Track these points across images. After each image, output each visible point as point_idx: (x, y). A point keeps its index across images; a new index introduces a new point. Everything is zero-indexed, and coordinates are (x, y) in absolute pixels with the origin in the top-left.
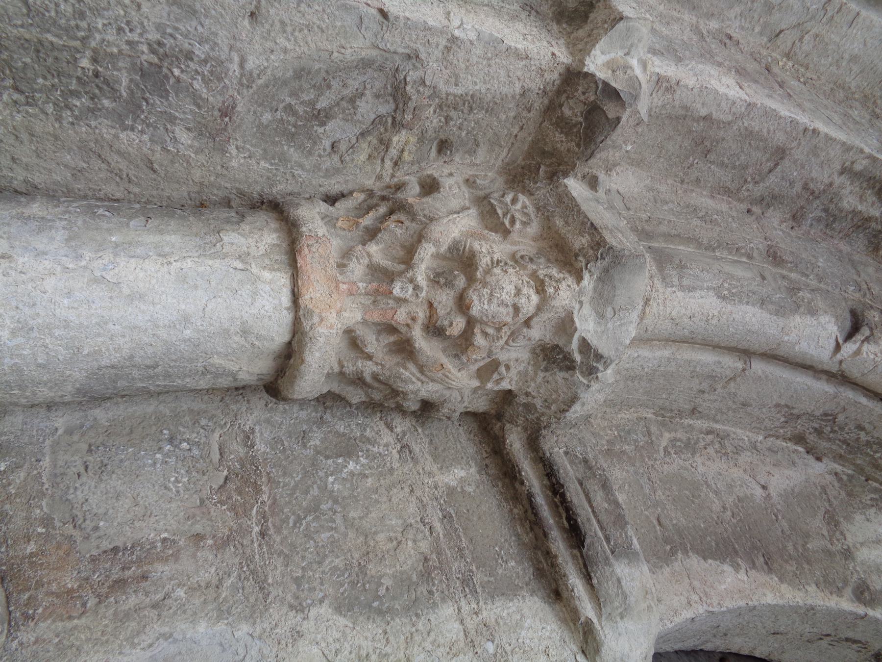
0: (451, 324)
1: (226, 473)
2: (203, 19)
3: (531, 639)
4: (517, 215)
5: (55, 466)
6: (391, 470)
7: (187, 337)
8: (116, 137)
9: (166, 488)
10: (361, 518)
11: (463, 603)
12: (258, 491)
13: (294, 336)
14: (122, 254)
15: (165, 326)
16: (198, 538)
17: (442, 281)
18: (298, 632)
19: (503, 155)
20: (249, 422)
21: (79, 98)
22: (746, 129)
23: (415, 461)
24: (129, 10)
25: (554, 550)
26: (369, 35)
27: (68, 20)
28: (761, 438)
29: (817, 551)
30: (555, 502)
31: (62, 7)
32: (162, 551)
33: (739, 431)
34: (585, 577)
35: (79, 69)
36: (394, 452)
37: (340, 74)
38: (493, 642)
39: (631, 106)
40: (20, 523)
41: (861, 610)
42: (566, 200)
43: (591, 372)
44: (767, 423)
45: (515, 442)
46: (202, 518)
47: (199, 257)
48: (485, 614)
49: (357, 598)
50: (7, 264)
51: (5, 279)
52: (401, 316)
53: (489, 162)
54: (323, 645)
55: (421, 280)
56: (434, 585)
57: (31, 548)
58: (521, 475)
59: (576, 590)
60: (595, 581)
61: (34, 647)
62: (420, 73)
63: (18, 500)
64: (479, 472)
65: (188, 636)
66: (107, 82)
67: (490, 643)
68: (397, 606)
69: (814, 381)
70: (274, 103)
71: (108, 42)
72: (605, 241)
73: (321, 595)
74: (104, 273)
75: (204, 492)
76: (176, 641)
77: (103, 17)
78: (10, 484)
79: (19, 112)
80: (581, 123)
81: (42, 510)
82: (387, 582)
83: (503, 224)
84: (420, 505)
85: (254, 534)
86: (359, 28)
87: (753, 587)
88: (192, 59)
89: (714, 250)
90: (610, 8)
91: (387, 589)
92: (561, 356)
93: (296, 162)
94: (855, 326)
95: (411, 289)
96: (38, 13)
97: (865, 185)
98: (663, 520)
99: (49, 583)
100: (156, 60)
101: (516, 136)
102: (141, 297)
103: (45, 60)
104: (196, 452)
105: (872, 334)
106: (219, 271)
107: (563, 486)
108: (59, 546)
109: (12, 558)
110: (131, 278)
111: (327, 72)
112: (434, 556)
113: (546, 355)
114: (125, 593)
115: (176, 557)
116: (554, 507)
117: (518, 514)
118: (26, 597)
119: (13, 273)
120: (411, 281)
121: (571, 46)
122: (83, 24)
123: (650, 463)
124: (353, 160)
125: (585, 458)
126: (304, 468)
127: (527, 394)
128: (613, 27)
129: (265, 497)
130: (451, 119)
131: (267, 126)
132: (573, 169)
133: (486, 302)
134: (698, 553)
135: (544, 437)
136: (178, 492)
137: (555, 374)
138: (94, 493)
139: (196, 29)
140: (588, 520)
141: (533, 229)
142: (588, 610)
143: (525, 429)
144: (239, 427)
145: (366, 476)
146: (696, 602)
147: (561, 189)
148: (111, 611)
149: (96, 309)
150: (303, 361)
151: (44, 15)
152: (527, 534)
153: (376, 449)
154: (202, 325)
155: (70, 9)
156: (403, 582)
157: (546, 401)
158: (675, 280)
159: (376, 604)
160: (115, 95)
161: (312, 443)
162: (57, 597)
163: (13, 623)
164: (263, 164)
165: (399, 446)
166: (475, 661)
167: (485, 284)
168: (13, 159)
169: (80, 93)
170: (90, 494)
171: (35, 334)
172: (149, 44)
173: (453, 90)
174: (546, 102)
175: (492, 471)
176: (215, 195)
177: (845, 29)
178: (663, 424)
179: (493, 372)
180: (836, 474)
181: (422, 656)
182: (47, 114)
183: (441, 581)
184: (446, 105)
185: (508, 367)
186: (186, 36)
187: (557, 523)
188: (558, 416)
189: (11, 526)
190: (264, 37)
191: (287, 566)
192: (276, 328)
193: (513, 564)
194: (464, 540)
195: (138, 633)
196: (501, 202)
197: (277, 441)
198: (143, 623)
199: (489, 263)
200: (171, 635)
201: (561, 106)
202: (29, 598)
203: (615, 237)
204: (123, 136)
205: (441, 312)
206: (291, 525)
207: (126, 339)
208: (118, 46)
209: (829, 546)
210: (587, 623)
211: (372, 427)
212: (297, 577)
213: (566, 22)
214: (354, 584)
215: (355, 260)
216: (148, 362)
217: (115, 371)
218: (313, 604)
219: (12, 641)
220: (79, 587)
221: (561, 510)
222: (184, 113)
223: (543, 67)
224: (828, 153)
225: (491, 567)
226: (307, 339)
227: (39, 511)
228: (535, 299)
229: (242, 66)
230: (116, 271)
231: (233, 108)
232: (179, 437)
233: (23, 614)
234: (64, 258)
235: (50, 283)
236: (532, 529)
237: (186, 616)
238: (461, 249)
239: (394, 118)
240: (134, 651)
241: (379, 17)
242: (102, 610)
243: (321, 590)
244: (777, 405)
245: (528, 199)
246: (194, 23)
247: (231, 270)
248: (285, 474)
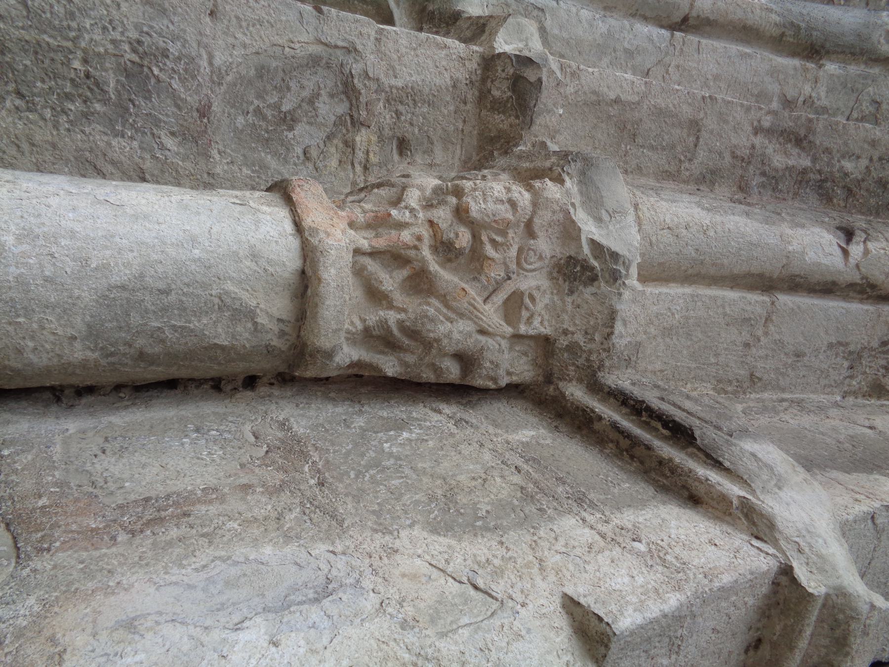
0: (457, 235)
2: (172, 17)
7: (197, 257)
8: (109, 144)
13: (305, 261)
24: (111, 9)
26: (310, 29)
27: (61, 21)
30: (645, 422)
34: (714, 466)
35: (72, 71)
37: (295, 73)
39: (545, 66)
43: (615, 277)
57: (43, 501)
59: (711, 478)
60: (727, 464)
66: (97, 84)
71: (96, 41)
77: (90, 17)
79: (20, 118)
80: (511, 97)
86: (301, 23)
88: (167, 57)
92: (578, 268)
93: (275, 169)
96: (36, 14)
97: (781, 139)
101: (463, 131)
102: (146, 217)
103: (43, 62)
111: (284, 71)
113: (565, 274)
116: (646, 426)
122: (74, 24)
124: (326, 166)
127: (565, 332)
130: (401, 114)
132: (521, 139)
139: (168, 27)
142: (735, 490)
143: (580, 380)
151: (41, 16)
152: (630, 464)
155: (62, 10)
157: (586, 333)
160: (105, 102)
169: (73, 96)
172: (130, 43)
173: (393, 82)
174: (477, 93)
177: (696, 56)
179: (520, 308)
182: (45, 120)
185: (532, 298)
186: (160, 35)
188: (606, 346)
201: (489, 91)
205: (443, 225)
207: (135, 254)
208: (104, 46)
210: (742, 503)
216: (161, 285)
217: (125, 295)
219: (22, 569)
221: (654, 423)
222: (167, 115)
223: (462, 55)
224: (734, 118)
226: (318, 254)
229: (211, 64)
231: (210, 107)
239: (351, 116)
244: (831, 346)
245: (475, 44)
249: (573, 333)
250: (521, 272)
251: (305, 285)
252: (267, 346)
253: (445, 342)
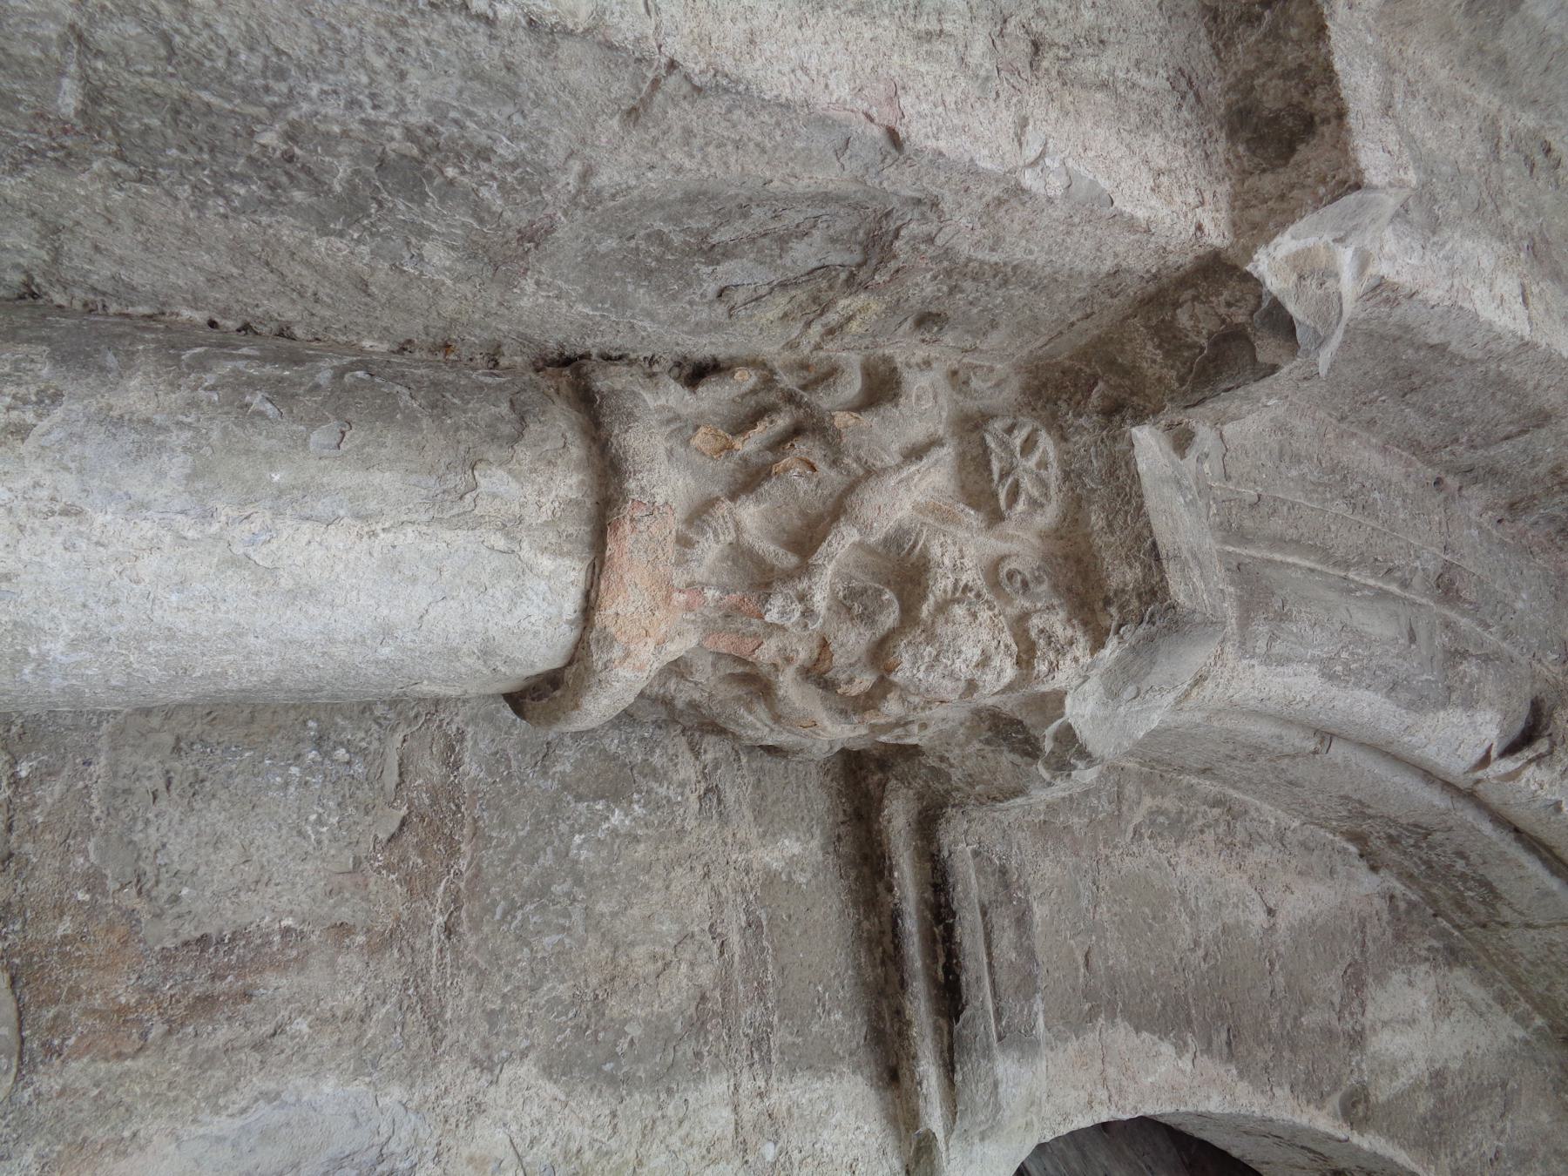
0: (850, 681)
1: (404, 811)
2: (528, 106)
3: (835, 1145)
4: (1027, 483)
5: (115, 774)
6: (681, 832)
8: (307, 242)
9: (300, 833)
10: (614, 915)
11: (745, 1077)
12: (453, 851)
13: (570, 663)
14: (289, 511)
15: (346, 641)
16: (343, 930)
17: (857, 608)
18: (479, 1105)
19: (1036, 344)
20: (457, 719)
21: (245, 183)
22: (1500, 374)
23: (724, 819)
25: (909, 1012)
28: (1296, 824)
29: (1313, 1030)
31: (243, 57)
32: (281, 952)
33: (1266, 807)
34: (945, 1065)
36: (693, 798)
38: (776, 1143)
39: (1308, 353)
40: (48, 880)
41: (1342, 1132)
42: (1122, 473)
44: (1317, 811)
45: (898, 815)
46: (353, 894)
47: (428, 524)
48: (775, 1096)
49: (581, 1054)
50: (73, 527)
51: (67, 555)
52: (767, 652)
54: (514, 1128)
55: (820, 601)
56: (706, 1043)
57: (65, 927)
58: (891, 874)
59: (925, 1085)
60: (958, 1077)
61: (59, 1102)
62: (931, 228)
63: (48, 837)
64: (824, 848)
65: (305, 1098)
67: (770, 1146)
68: (641, 1074)
69: (1422, 785)
72: (1165, 589)
73: (525, 1043)
74: (250, 550)
75: (363, 846)
76: (284, 1105)
78: (34, 806)
80: (1202, 349)
81: (87, 858)
82: (634, 1030)
83: (995, 495)
84: (714, 900)
85: (434, 931)
87: (1195, 1083)
89: (1348, 568)
90: (1345, 152)
91: (632, 1042)
94: (1526, 736)
95: (797, 614)
98: (1094, 959)
99: (90, 993)
100: (415, 152)
104: (359, 768)
105: (1551, 752)
106: (461, 552)
107: (954, 915)
108: (110, 929)
109: (32, 944)
110: (300, 559)
112: (717, 994)
114: (212, 1019)
115: (302, 963)
116: (929, 941)
117: (869, 931)
118: (51, 1015)
119: (82, 544)
120: (802, 598)
121: (1241, 202)
123: (1104, 851)
125: (1003, 866)
126: (536, 815)
128: (1335, 199)
129: (463, 864)
131: (604, 256)
133: (923, 668)
134: (1130, 1020)
135: (948, 822)
136: (319, 842)
137: (1001, 752)
138: (177, 834)
140: (978, 979)
141: (1048, 517)
142: (934, 1118)
143: (920, 797)
144: (440, 727)
145: (637, 839)
146: (1101, 1103)
147: (1122, 446)
148: (186, 1050)
149: (227, 612)
150: (577, 706)
151: (200, 64)
152: (874, 967)
153: (662, 791)
156: (661, 1033)
158: (1261, 645)
159: (608, 1067)
161: (559, 768)
162: (102, 1019)
163: (27, 1059)
164: (580, 307)
165: (703, 786)
166: (741, 1175)
167: (931, 638)
168: (96, 248)
169: (250, 177)
170: (172, 834)
171: (111, 646)
175: (844, 849)
178: (1147, 781)
180: (1392, 897)
181: (663, 1158)
182: (176, 198)
183: (718, 1038)
187: (927, 967)
189: (32, 885)
190: (642, 147)
191: (479, 990)
192: (543, 650)
193: (838, 1016)
194: (770, 967)
195: (226, 1090)
196: (1005, 445)
197: (500, 757)
198: (235, 1074)
199: (950, 587)
200: (278, 1095)
201: (1176, 305)
202: (55, 1018)
203: (1187, 580)
204: (320, 243)
205: (839, 659)
206: (498, 917)
208: (343, 124)
209: (1335, 1022)
211: (665, 748)
212: (493, 1011)
213: (1247, 141)
214: (580, 1030)
215: (710, 535)
218: (508, 1060)
219: (24, 1088)
220: (139, 1002)
221: (940, 948)
225: (803, 1019)
227: (82, 860)
228: (1010, 673)
230: (274, 545)
232: (333, 736)
233: (43, 1045)
234: (179, 517)
235: (149, 565)
236: (883, 963)
237: (305, 1066)
238: (907, 547)
240: (216, 1119)
241: (884, 142)
242: (172, 1046)
243: (527, 1036)
244: (1346, 797)
245: (1056, 445)
246: (509, 109)
247: (484, 551)
248: (503, 823)
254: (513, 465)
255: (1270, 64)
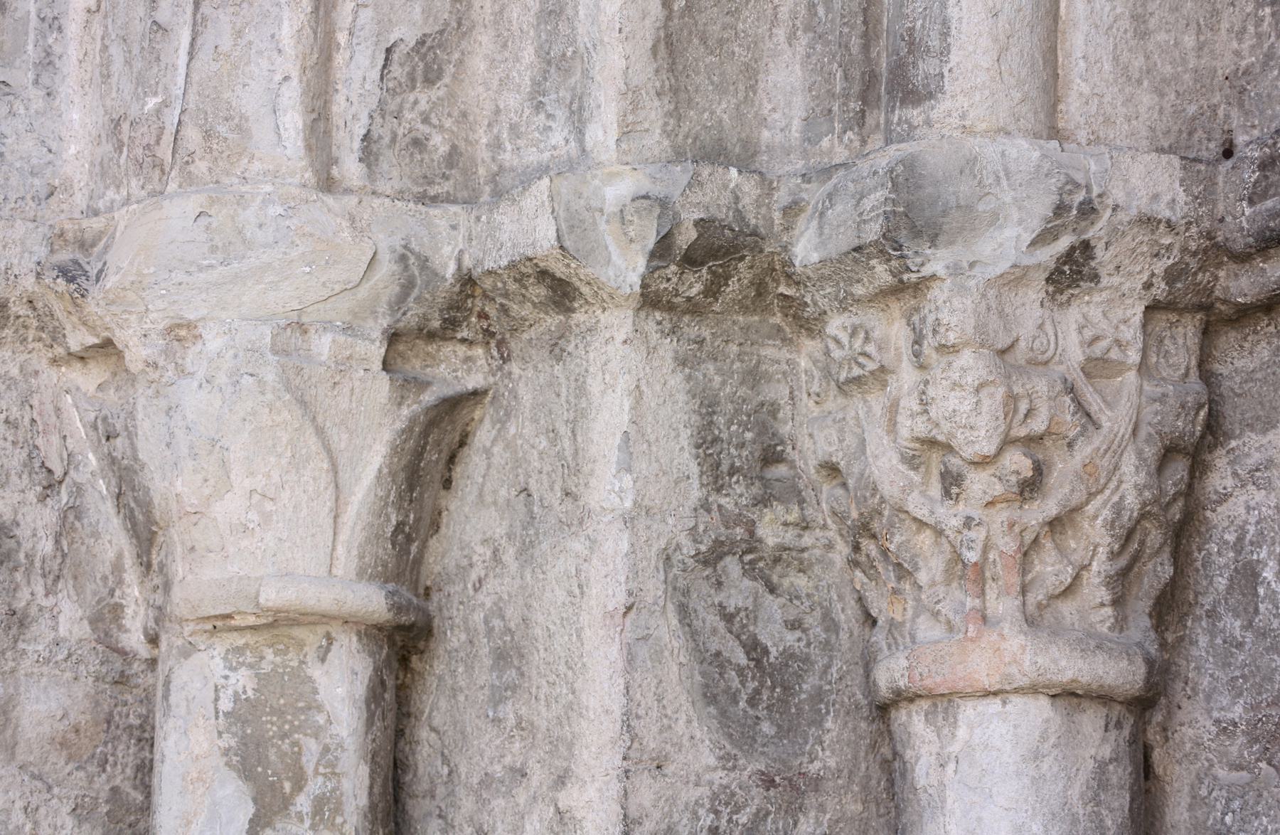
1: (1263, 765)
45: (1241, 285)
53: (784, 373)
70: (749, 722)
80: (709, 268)
92: (1066, 268)
93: (821, 679)
104: (1236, 804)
124: (808, 595)
126: (1267, 650)
127: (1148, 286)
131: (779, 726)
133: (976, 434)
144: (1212, 740)
153: (1252, 529)
154: (1026, 811)
157: (1156, 255)
161: (1237, 633)
164: (829, 724)
165: (1251, 487)
174: (686, 319)
176: (879, 783)
179: (1106, 361)
184: (716, 482)
188: (1183, 228)
201: (689, 299)
205: (998, 489)
231: (763, 774)
232: (1218, 827)
241: (632, 614)
249: (1153, 275)
250: (1057, 358)
251: (1069, 696)
252: (1130, 745)
253: (1147, 494)
254: (913, 761)
255: (524, 296)
